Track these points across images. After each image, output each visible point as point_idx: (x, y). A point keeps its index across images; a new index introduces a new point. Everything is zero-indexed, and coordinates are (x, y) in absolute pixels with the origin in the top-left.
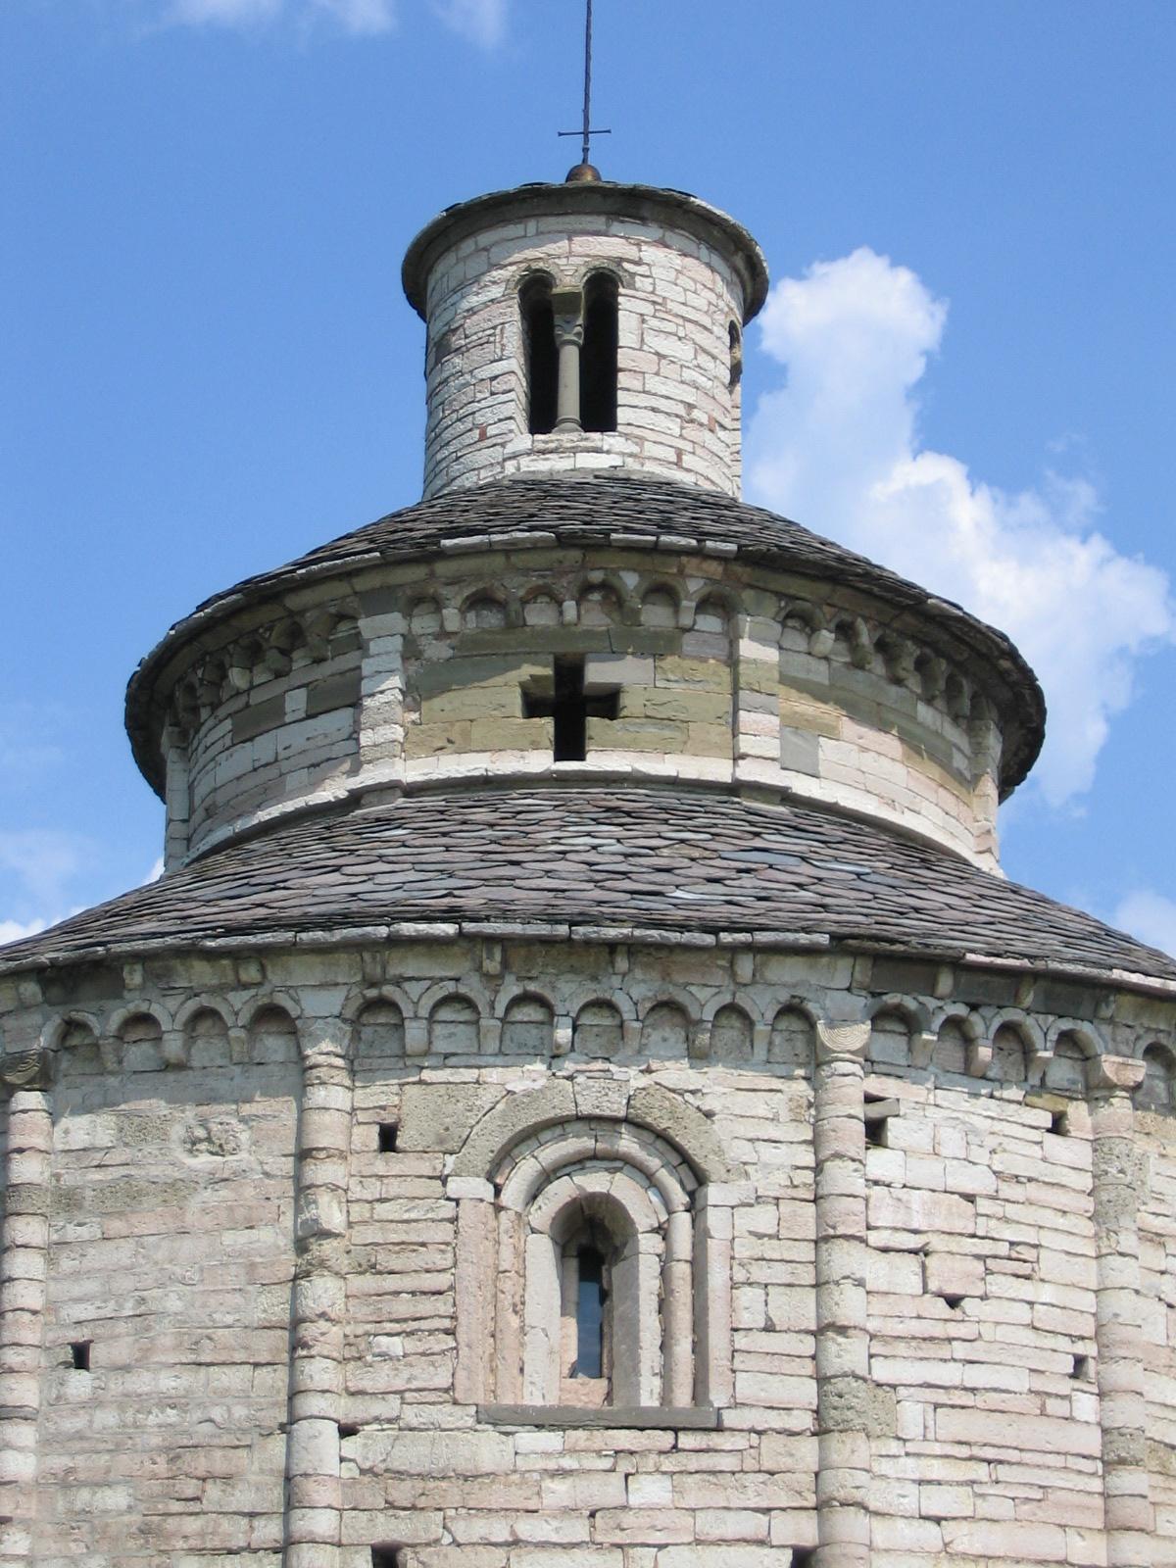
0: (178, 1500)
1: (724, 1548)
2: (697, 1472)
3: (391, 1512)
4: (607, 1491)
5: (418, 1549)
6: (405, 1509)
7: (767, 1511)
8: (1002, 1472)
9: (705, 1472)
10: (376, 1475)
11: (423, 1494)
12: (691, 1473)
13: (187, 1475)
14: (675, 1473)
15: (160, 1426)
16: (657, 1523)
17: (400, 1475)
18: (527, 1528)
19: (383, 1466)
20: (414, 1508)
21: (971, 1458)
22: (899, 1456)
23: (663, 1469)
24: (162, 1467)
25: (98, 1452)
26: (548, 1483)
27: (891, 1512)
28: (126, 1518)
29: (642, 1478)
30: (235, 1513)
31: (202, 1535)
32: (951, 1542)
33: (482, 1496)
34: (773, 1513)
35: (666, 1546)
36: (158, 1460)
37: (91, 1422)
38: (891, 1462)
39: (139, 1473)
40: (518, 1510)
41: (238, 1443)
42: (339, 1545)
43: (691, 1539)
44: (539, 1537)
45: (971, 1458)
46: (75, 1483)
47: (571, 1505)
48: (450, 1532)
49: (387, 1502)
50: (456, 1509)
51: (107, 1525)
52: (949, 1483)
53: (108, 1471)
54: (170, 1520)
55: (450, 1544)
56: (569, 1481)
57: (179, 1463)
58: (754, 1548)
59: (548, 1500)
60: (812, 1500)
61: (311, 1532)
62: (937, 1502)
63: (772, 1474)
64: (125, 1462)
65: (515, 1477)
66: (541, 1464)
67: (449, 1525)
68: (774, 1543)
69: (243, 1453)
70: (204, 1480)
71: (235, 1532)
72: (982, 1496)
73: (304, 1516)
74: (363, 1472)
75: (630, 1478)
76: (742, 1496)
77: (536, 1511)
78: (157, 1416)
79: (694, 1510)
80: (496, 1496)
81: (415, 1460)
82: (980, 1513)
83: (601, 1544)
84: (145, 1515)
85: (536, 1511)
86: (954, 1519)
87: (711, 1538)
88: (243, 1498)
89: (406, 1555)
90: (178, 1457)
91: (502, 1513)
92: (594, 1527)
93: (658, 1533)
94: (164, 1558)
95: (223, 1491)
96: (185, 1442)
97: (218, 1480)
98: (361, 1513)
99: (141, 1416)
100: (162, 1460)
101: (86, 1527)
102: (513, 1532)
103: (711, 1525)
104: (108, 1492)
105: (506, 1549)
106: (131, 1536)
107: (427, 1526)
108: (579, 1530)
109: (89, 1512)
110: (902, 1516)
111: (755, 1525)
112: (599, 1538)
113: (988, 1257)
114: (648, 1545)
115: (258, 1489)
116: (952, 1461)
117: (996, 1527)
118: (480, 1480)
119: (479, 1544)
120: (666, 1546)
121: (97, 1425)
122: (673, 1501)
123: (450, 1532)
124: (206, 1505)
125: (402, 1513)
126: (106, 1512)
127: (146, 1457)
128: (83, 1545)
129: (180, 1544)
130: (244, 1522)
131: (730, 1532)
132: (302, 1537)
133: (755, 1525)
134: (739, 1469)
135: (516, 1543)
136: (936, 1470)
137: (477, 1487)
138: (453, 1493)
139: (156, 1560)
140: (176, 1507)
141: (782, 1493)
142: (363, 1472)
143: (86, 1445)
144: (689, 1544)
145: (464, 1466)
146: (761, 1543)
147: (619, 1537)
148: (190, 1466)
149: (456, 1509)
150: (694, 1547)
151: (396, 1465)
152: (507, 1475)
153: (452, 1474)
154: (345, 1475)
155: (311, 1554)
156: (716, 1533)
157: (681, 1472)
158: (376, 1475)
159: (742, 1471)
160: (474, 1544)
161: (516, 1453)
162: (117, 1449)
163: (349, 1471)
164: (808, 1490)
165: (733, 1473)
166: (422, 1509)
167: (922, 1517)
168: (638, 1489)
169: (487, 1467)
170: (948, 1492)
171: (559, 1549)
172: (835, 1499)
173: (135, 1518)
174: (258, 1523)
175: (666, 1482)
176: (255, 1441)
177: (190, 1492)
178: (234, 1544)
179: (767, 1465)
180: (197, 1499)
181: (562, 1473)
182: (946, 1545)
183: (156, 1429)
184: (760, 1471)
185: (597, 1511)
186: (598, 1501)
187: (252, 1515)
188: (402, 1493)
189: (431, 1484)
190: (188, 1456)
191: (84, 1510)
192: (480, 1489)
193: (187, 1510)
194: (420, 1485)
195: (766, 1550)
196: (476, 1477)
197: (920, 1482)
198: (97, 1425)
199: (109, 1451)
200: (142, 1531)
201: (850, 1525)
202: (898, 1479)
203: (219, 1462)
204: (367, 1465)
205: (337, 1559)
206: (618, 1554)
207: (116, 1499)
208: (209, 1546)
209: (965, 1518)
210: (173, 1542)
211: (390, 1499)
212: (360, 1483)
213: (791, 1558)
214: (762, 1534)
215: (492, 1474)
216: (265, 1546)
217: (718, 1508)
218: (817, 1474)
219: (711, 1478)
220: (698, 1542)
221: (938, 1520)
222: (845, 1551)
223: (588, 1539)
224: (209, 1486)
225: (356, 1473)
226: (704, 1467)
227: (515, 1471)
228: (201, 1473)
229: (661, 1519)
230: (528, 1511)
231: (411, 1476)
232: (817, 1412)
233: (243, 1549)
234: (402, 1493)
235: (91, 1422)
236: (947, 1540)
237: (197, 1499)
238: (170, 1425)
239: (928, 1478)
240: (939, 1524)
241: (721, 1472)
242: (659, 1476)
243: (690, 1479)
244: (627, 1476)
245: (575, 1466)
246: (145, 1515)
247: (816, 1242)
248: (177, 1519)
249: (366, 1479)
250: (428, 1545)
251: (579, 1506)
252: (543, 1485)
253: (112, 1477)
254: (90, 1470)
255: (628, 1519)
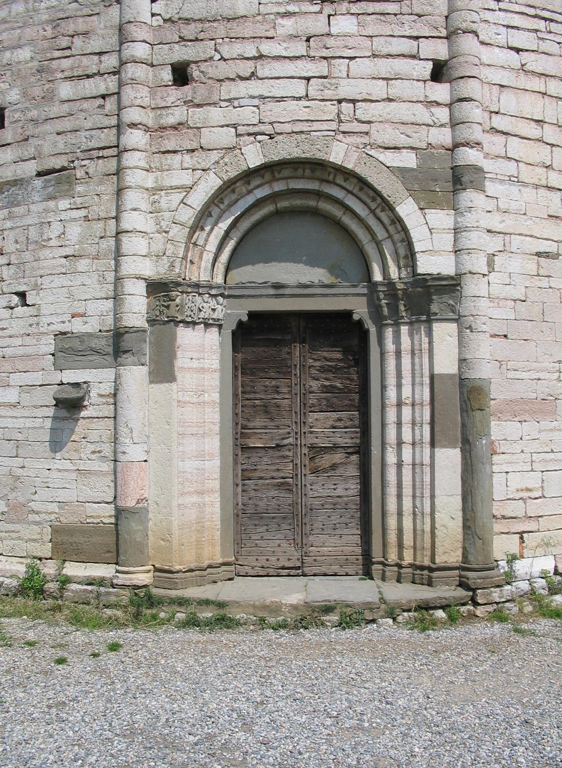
0: (58, 50)
1: (391, 60)
2: (373, 14)
3: (183, 43)
4: (318, 25)
5: (199, 64)
6: (191, 41)
7: (417, 38)
8: (553, 27)
9: (378, 14)
10: (173, 22)
11: (202, 31)
12: (369, 14)
13: (63, 35)
14: (359, 14)
15: (47, 8)
16: (349, 44)
17: (187, 21)
18: (267, 48)
19: (177, 16)
20: (197, 40)
21: (536, 16)
22: (495, 10)
23: (352, 11)
24: (49, 33)
25: (14, 29)
26: (280, 21)
27: (491, 43)
28: (30, 65)
29: (338, 17)
30: (90, 54)
31: (72, 69)
32: (525, 64)
33: (238, 29)
34: (420, 40)
35: (355, 58)
36: (47, 28)
37: (10, 12)
38: (491, 13)
39: (36, 38)
40: (261, 38)
41: (92, 13)
42: (152, 66)
43: (371, 54)
44: (275, 53)
45: (536, 16)
46: (3, 49)
47: (295, 34)
48: (219, 53)
49: (180, 37)
50: (223, 39)
51: (20, 70)
52: (523, 29)
53: (20, 39)
54: (54, 62)
55: (219, 60)
56: (293, 19)
57: (58, 29)
58: (409, 60)
59: (280, 31)
60: (444, 33)
61: (133, 56)
62: (519, 39)
63: (420, 16)
64: (29, 33)
65: (259, 18)
66: (276, 9)
67: (218, 48)
68: (421, 57)
69: (95, 18)
70: (73, 36)
71: (91, 64)
72: (543, 39)
73: (128, 46)
74: (165, 21)
75: (331, 17)
76: (401, 29)
77: (273, 38)
78: (46, 3)
79: (371, 37)
80: (248, 29)
81: (197, 11)
82: (541, 49)
83: (314, 57)
84: (40, 62)
85: (273, 38)
86: (527, 51)
87: (382, 53)
88: (95, 44)
89: (192, 68)
90: (58, 25)
91: (252, 40)
92: (309, 47)
93: (349, 51)
94: (51, 85)
95: (84, 42)
96: (62, 16)
97: (80, 36)
98: (165, 46)
99: (37, 4)
100: (49, 28)
101: (9, 73)
102: (258, 51)
103: (380, 45)
104: (20, 51)
105: (254, 61)
106: (33, 74)
107: (205, 49)
108: (300, 48)
109: (10, 64)
110: (497, 46)
111: (408, 46)
112: (312, 54)
113: (503, 158)
114: (344, 58)
115: (103, 38)
116: (525, 17)
117: (550, 58)
118: (237, 21)
119: (237, 59)
120: (355, 58)
121: (13, 14)
122: (358, 31)
123: (219, 53)
124: (74, 52)
125: (189, 43)
126: (19, 62)
127: (40, 28)
128: (7, 84)
129: (60, 75)
130: (96, 58)
131: (394, 50)
132: (127, 59)
133: (408, 46)
134: (399, 12)
135: (261, 57)
136: (517, 20)
137: (236, 25)
138: (221, 29)
139: (47, 86)
140: (57, 54)
141: (426, 28)
142: (165, 21)
143: (7, 26)
144: (369, 57)
145: (230, 13)
146: (413, 57)
147: (325, 53)
148: (64, 30)
149: (223, 39)
150: (371, 59)
151: (186, 15)
152: (254, 16)
153: (220, 18)
154: (155, 24)
155: (133, 69)
156: (385, 51)
157: (363, 14)
158: (173, 22)
159: (401, 14)
160: (234, 59)
161: (260, 4)
162: (25, 25)
163: (157, 21)
164: (442, 27)
165: (395, 15)
166: (202, 40)
167: (509, 48)
168: (337, 24)
169: (242, 13)
170: (523, 34)
171: (287, 61)
172: (460, 29)
173: (35, 64)
174: (104, 58)
175: (354, 19)
176: (102, 10)
177: (64, 45)
178: (89, 72)
179: (417, 10)
180: (69, 48)
181: (288, 14)
182: (522, 65)
183: (45, 11)
184: (412, 14)
185: (311, 37)
186: (312, 31)
187: (100, 54)
188: (189, 31)
189: (207, 25)
190: (63, 23)
191: (8, 64)
192: (238, 26)
193: (63, 55)
194: (200, 26)
195: (416, 62)
196: (234, 19)
197: (508, 27)
198: (13, 14)
199: (20, 27)
200: (38, 71)
201: (467, 43)
202: (495, 23)
203: (81, 25)
204: (167, 17)
205: (151, 74)
206: (325, 63)
207: (25, 54)
208: (76, 74)
209: (533, 51)
210: (56, 75)
211: (182, 35)
212: (163, 28)
213: (432, 67)
214: (414, 52)
215: (245, 16)
216: (108, 71)
217: (387, 36)
218: (447, 17)
219: (382, 18)
220: (374, 56)
221: (518, 51)
222: (467, 60)
223: (305, 54)
224: (76, 39)
225: (161, 22)
226: (378, 11)
227: (259, 14)
228: (71, 32)
229: (351, 42)
230: (267, 38)
231: (195, 21)
232: (447, 17)
233: (95, 74)
234: (189, 31)
235: (10, 12)
236: (523, 63)
237: (69, 48)
238: (53, 7)
239: (512, 25)
240: (518, 53)
241: (388, 14)
242: (349, 16)
243: (369, 18)
244: (329, 16)
245: (297, 10)
246: (40, 62)
247: (451, 104)
248: (57, 61)
249: (167, 25)
250: (205, 61)
251: (300, 35)
252: (276, 22)
253: (22, 42)
254: (10, 39)
255: (330, 42)
